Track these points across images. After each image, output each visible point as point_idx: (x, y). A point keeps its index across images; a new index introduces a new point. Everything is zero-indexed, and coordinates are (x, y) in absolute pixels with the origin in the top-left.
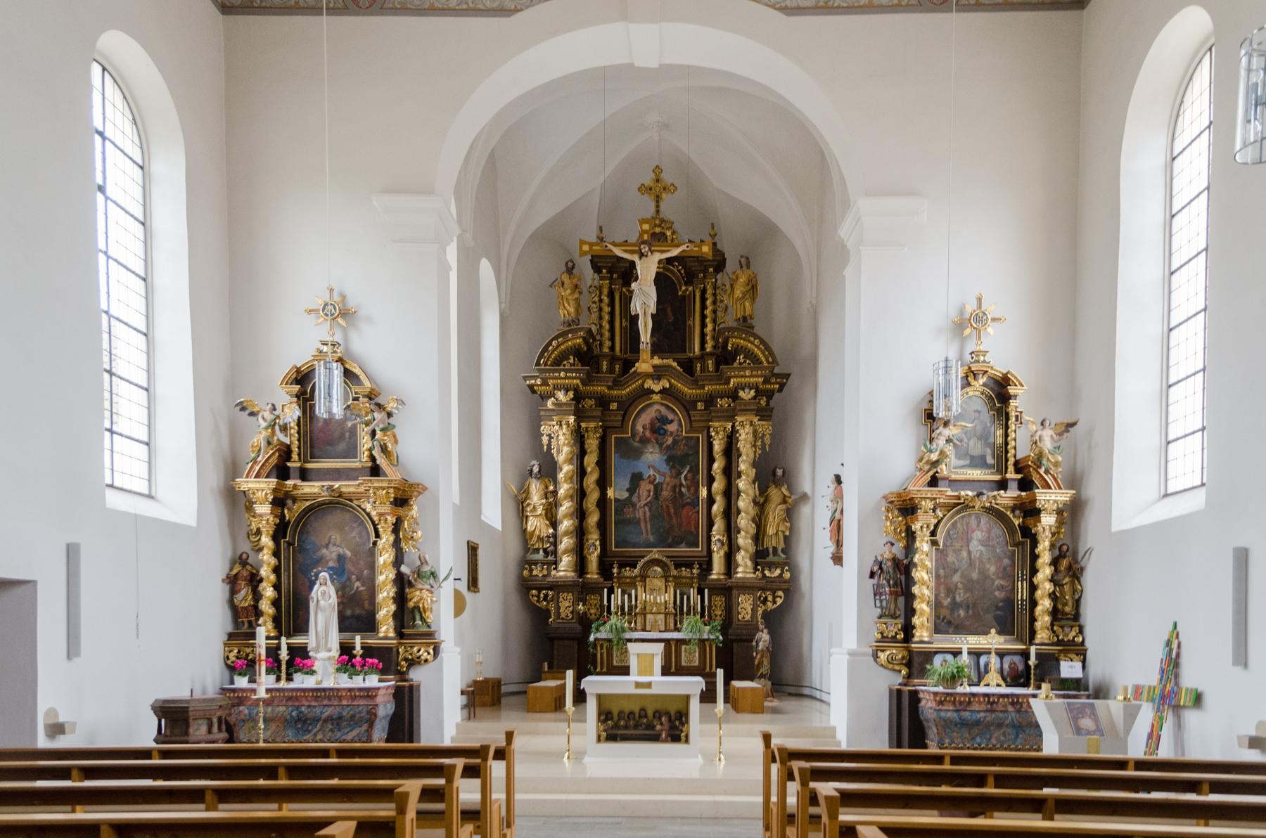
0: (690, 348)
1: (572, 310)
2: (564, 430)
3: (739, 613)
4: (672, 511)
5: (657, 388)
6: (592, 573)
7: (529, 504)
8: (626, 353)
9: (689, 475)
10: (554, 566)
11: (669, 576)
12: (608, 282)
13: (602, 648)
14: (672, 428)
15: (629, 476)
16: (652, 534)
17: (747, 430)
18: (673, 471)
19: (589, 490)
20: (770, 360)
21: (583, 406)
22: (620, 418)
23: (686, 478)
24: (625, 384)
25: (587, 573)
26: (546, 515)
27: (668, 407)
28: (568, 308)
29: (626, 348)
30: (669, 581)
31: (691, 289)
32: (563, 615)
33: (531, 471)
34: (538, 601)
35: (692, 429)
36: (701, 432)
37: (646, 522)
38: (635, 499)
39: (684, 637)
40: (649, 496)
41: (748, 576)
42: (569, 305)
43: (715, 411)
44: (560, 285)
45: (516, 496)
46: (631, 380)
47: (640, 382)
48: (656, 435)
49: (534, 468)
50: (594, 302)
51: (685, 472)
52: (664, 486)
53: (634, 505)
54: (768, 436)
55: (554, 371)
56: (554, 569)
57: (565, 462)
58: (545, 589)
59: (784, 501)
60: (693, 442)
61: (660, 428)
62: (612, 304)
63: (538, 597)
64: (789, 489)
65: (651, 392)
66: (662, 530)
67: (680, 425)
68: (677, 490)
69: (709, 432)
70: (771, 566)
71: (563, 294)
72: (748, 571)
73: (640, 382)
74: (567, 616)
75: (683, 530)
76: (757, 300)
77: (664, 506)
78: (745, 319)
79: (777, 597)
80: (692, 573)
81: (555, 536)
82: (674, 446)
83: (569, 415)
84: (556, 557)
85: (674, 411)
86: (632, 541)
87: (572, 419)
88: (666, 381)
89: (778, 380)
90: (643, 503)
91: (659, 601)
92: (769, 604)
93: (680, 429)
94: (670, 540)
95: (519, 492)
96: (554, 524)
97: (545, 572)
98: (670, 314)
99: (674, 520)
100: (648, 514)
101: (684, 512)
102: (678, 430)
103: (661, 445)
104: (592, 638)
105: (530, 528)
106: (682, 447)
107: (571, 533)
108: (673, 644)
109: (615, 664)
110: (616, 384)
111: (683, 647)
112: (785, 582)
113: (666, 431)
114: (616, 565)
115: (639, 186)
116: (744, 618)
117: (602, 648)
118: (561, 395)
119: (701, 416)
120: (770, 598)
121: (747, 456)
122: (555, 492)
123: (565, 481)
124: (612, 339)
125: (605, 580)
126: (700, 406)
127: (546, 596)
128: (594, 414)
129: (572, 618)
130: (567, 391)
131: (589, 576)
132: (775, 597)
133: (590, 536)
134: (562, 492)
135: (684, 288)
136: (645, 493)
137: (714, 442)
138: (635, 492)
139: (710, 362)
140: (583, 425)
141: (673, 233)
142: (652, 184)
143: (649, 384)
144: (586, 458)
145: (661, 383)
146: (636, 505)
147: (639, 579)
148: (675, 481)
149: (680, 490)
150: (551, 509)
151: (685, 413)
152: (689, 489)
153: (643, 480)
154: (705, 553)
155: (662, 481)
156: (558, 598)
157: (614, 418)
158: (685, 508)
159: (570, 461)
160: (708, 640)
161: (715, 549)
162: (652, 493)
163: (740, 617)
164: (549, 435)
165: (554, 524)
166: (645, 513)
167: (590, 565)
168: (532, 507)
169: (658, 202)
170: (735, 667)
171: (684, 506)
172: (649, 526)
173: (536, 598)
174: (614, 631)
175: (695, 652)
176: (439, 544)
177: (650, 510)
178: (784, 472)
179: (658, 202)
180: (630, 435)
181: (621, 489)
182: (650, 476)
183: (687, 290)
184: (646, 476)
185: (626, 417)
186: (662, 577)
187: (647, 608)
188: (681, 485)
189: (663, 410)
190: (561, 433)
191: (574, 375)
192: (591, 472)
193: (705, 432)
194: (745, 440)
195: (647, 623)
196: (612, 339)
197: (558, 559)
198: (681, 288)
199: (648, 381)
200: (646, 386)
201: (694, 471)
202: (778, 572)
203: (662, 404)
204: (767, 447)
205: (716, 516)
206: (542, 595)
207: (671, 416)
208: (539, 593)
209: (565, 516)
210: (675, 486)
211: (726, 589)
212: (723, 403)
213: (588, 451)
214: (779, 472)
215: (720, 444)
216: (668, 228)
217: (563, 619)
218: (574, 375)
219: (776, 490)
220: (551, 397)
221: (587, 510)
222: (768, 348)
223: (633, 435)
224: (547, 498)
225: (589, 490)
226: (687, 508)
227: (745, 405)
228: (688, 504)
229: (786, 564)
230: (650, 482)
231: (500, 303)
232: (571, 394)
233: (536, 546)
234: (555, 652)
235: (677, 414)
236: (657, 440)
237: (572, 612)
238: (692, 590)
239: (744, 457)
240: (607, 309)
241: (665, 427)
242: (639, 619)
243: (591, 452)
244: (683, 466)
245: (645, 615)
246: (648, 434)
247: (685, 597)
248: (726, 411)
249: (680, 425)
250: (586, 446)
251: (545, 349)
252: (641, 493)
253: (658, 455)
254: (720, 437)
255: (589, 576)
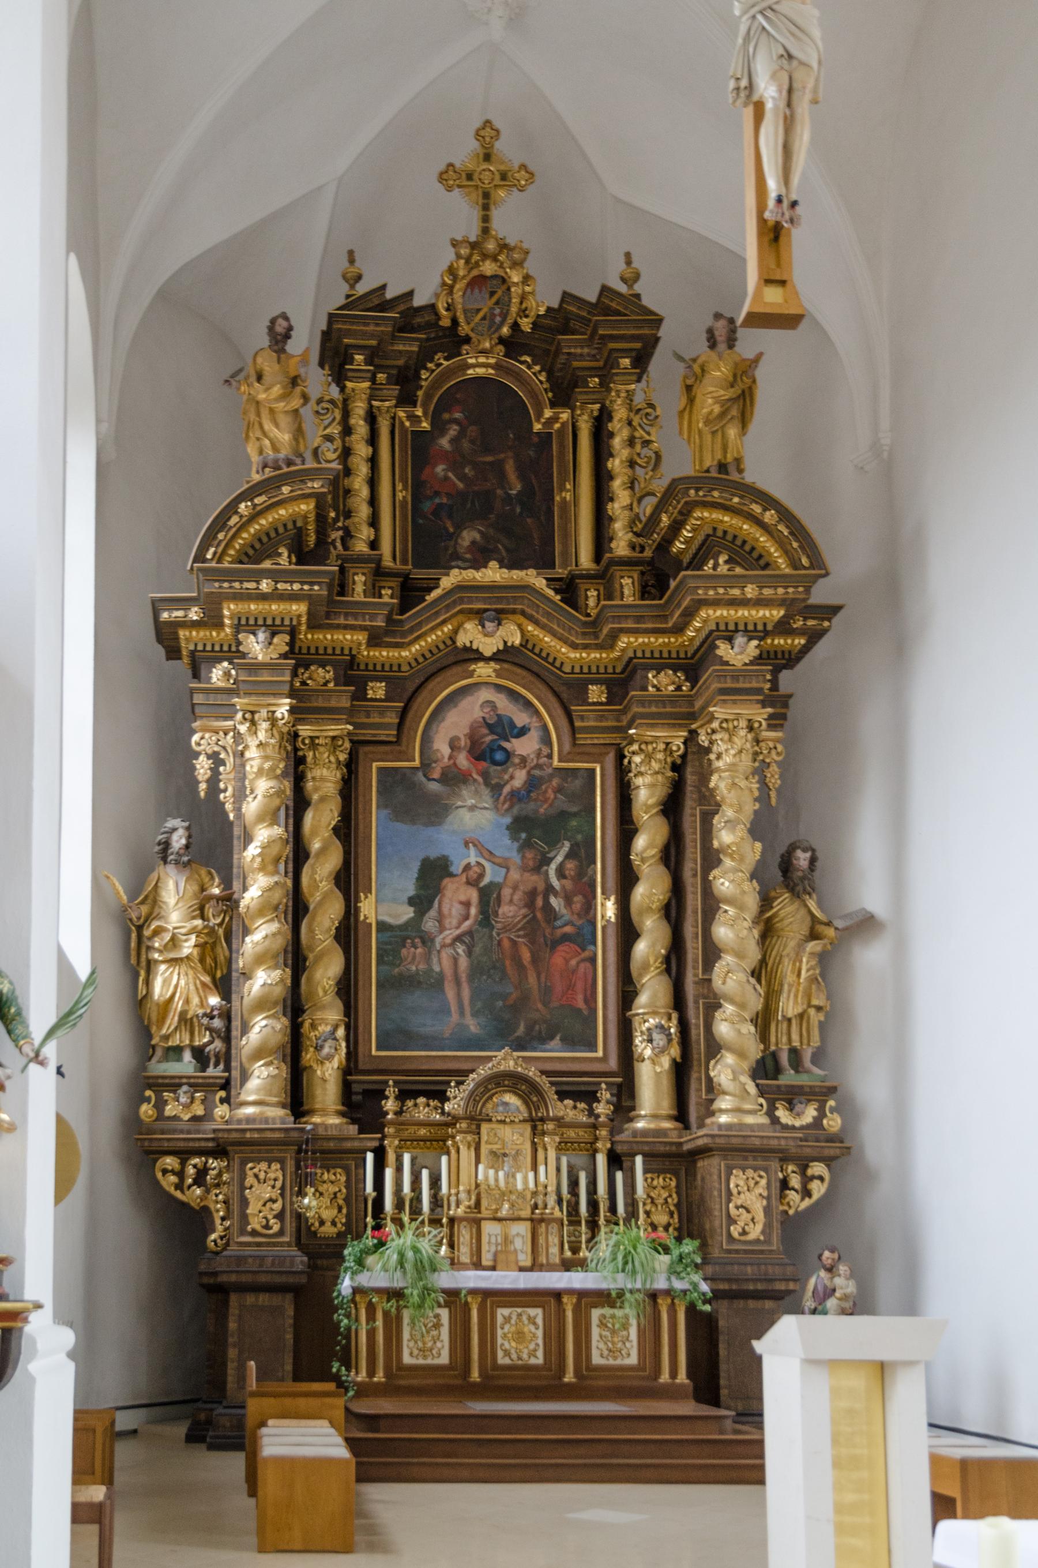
0: (565, 554)
1: (284, 437)
2: (262, 735)
3: (731, 1221)
4: (526, 955)
5: (489, 646)
6: (324, 1112)
7: (157, 932)
8: (404, 562)
9: (570, 865)
10: (222, 1094)
11: (542, 1120)
12: (367, 384)
13: (371, 1317)
14: (525, 747)
15: (415, 867)
16: (475, 1014)
17: (738, 742)
18: (529, 855)
19: (318, 896)
20: (805, 561)
21: (304, 683)
22: (393, 719)
23: (561, 873)
24: (412, 630)
25: (310, 1112)
26: (202, 960)
27: (513, 695)
28: (274, 432)
29: (404, 552)
30: (544, 1133)
31: (565, 415)
32: (255, 1224)
33: (166, 845)
34: (179, 1186)
35: (577, 751)
36: (599, 758)
37: (458, 983)
38: (429, 924)
39: (604, 1286)
40: (466, 917)
41: (750, 1120)
42: (277, 426)
43: (642, 703)
44: (253, 378)
45: (124, 910)
46: (428, 620)
47: (448, 628)
48: (484, 765)
49: (175, 837)
50: (329, 438)
51: (559, 859)
52: (506, 892)
53: (427, 940)
54: (774, 768)
55: (242, 576)
56: (222, 1101)
57: (260, 818)
58: (200, 1153)
59: (814, 935)
60: (578, 784)
61: (492, 749)
62: (373, 440)
63: (181, 1174)
64: (820, 905)
65: (472, 655)
66: (500, 1003)
67: (547, 740)
68: (539, 902)
69: (620, 756)
70: (792, 1097)
71: (262, 396)
72: (748, 1106)
73: (448, 628)
74: (267, 1227)
75: (555, 1004)
76: (753, 427)
77: (506, 944)
78: (722, 467)
79: (813, 1178)
80: (591, 1112)
81: (227, 1016)
82: (529, 792)
83: (280, 695)
84: (228, 1068)
85: (528, 704)
86: (423, 1030)
87: (283, 708)
88: (513, 627)
89: (811, 623)
90: (449, 935)
91: (520, 1186)
92: (793, 1196)
93: (546, 751)
94: (521, 1030)
95: (132, 897)
96: (224, 985)
97: (200, 1111)
98: (512, 475)
99: (532, 979)
100: (464, 963)
101: (558, 959)
102: (539, 754)
103: (496, 789)
104: (346, 1285)
105: (159, 989)
106: (551, 795)
107: (275, 1004)
108: (568, 1303)
109: (407, 1359)
110: (375, 640)
111: (596, 1313)
112: (832, 1138)
113: (508, 755)
114: (391, 1091)
115: (442, 167)
116: (744, 1233)
117: (371, 1317)
118: (256, 646)
119: (601, 718)
120: (795, 1181)
121: (739, 810)
122: (229, 902)
123: (262, 869)
124: (374, 522)
125: (360, 1132)
126: (596, 693)
127: (201, 1174)
128: (333, 703)
129: (281, 1233)
130: (274, 634)
131: (317, 1119)
132: (806, 1180)
133: (319, 1015)
134: (252, 895)
135: (548, 413)
136: (457, 910)
137: (639, 781)
138: (430, 907)
139: (626, 581)
140: (305, 730)
141: (527, 279)
142: (471, 166)
143: (470, 634)
144: (309, 818)
145: (502, 632)
146: (432, 940)
147: (464, 1125)
148: (534, 880)
149: (547, 905)
150: (214, 946)
151: (559, 712)
152: (568, 901)
153: (451, 875)
154: (613, 1064)
155: (499, 879)
156: (243, 1176)
157: (377, 720)
158: (561, 948)
159: (269, 816)
160: (668, 1292)
161: (648, 1052)
162: (473, 911)
163: (735, 1231)
164: (214, 756)
165: (224, 985)
166: (455, 960)
167: (318, 1092)
168: (167, 937)
169: (486, 207)
170: (723, 1367)
171: (554, 944)
172: (466, 993)
173: (173, 1179)
174: (408, 1266)
175: (625, 1326)
176: (28, 874)
177: (469, 953)
178: (813, 860)
179: (486, 207)
180: (417, 763)
181: (394, 900)
182: (467, 867)
183: (555, 419)
184: (457, 868)
185: (411, 715)
186: (525, 1121)
187: (484, 1203)
188: (549, 889)
189: (504, 705)
190: (252, 742)
191: (296, 586)
192: (323, 851)
193: (610, 758)
194: (732, 767)
195: (485, 1247)
196: (374, 522)
197: (235, 1074)
198: (539, 415)
199: (469, 626)
200: (462, 640)
201: (585, 853)
202: (810, 1113)
203: (499, 688)
204: (773, 794)
205: (645, 967)
206: (191, 1171)
207: (521, 718)
208: (183, 1163)
209: (260, 960)
210: (532, 894)
211: (680, 1155)
212: (664, 682)
213: (315, 797)
214: (802, 859)
215: (652, 786)
216: (516, 264)
217: (254, 1233)
218: (296, 586)
219: (796, 905)
220: (220, 660)
221: (311, 949)
222: (798, 530)
223: (426, 766)
224: (203, 917)
225: (318, 896)
226: (563, 949)
227: (735, 678)
228: (566, 938)
229: (832, 1091)
230: (468, 883)
231: (98, 421)
232: (281, 642)
233: (172, 1042)
234: (232, 1326)
235: (537, 712)
236: (485, 775)
237: (280, 1216)
238: (444, 1159)
239: (729, 812)
240: (362, 450)
241: (506, 745)
242: (464, 1235)
243: (323, 799)
244: (553, 843)
245: (477, 1222)
246: (463, 761)
247: (425, 1173)
248: (671, 700)
249: (547, 740)
250: (309, 785)
251: (220, 523)
252: (445, 910)
253: (489, 815)
254: (656, 766)
255: (317, 1119)
